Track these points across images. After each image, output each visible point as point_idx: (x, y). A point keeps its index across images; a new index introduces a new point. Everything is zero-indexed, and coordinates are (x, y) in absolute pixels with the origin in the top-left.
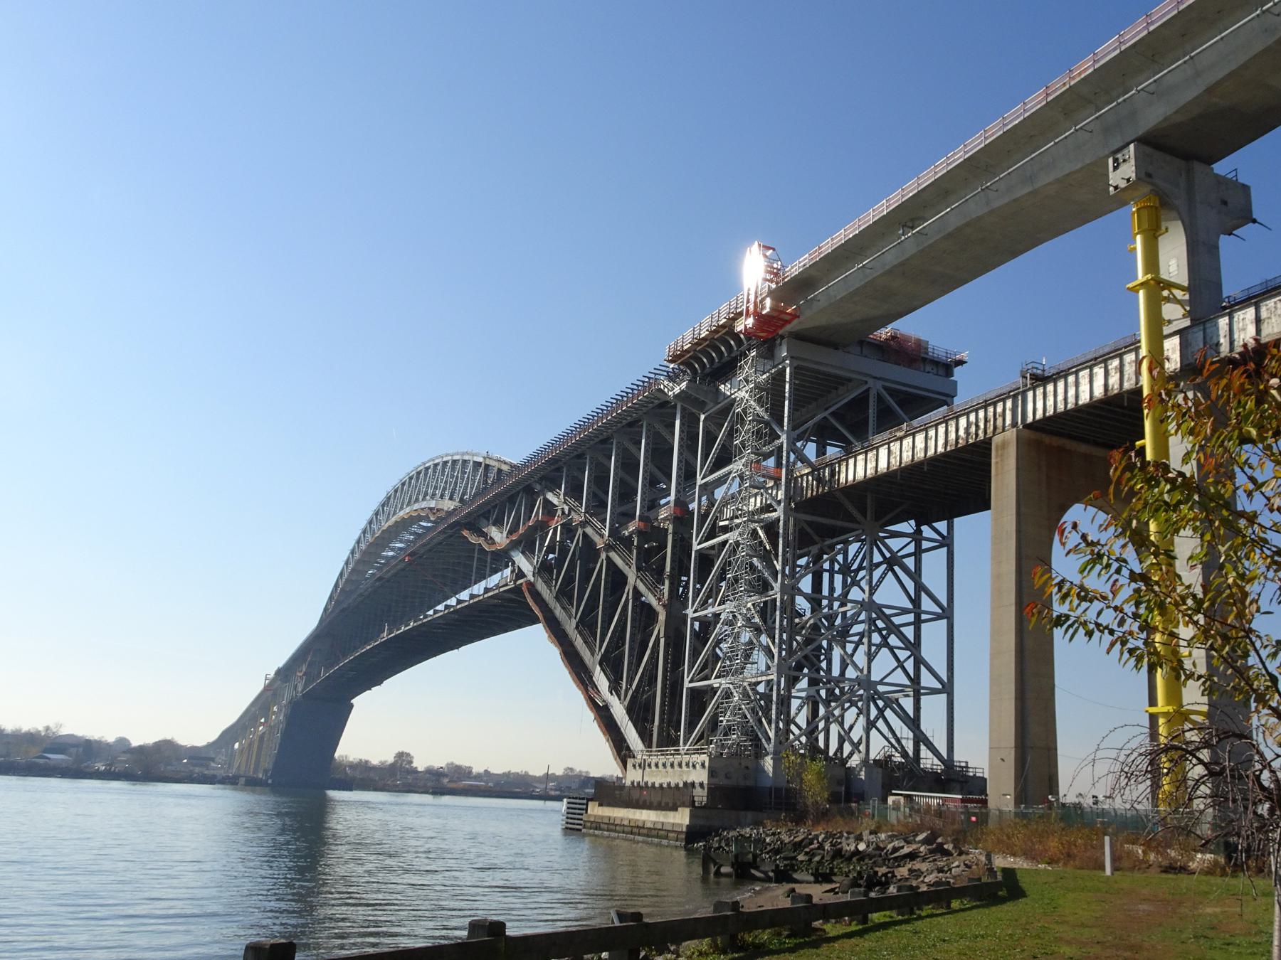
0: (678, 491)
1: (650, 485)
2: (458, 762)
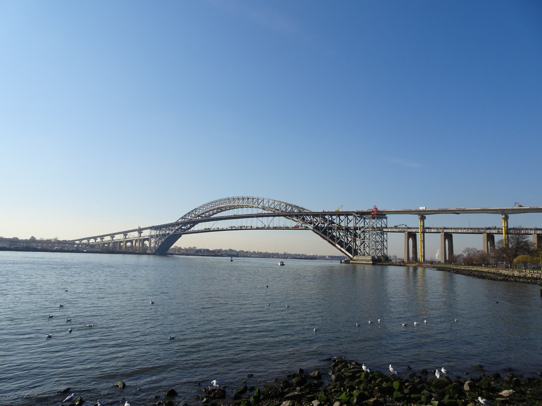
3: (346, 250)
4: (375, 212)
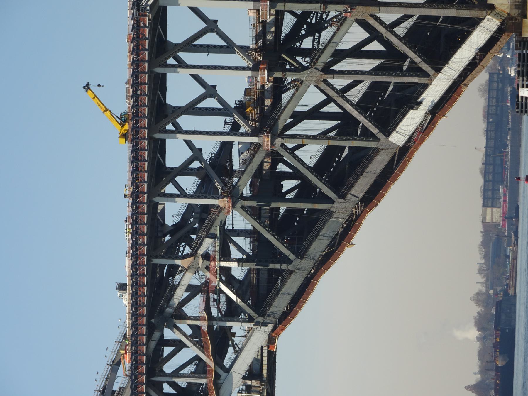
3: (438, 70)
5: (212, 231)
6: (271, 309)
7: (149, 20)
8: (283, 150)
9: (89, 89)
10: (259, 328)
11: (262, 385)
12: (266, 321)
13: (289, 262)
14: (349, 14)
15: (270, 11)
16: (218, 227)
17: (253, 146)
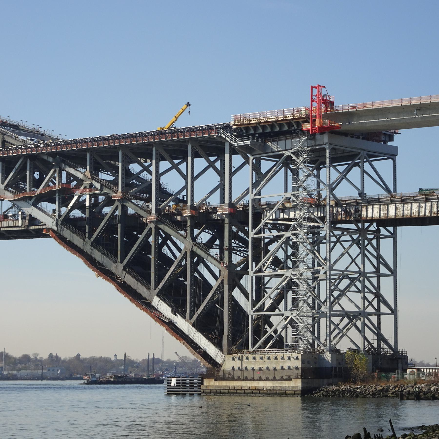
0: (123, 191)
1: (125, 186)
2: (24, 354)
3: (193, 325)
4: (320, 116)
5: (104, 188)
6: (65, 228)
7: (213, 136)
8: (148, 229)
9: (188, 106)
10: (55, 222)
11: (26, 226)
12: (59, 226)
13: (90, 238)
14: (222, 265)
15: (224, 214)
16: (106, 192)
17: (150, 210)
